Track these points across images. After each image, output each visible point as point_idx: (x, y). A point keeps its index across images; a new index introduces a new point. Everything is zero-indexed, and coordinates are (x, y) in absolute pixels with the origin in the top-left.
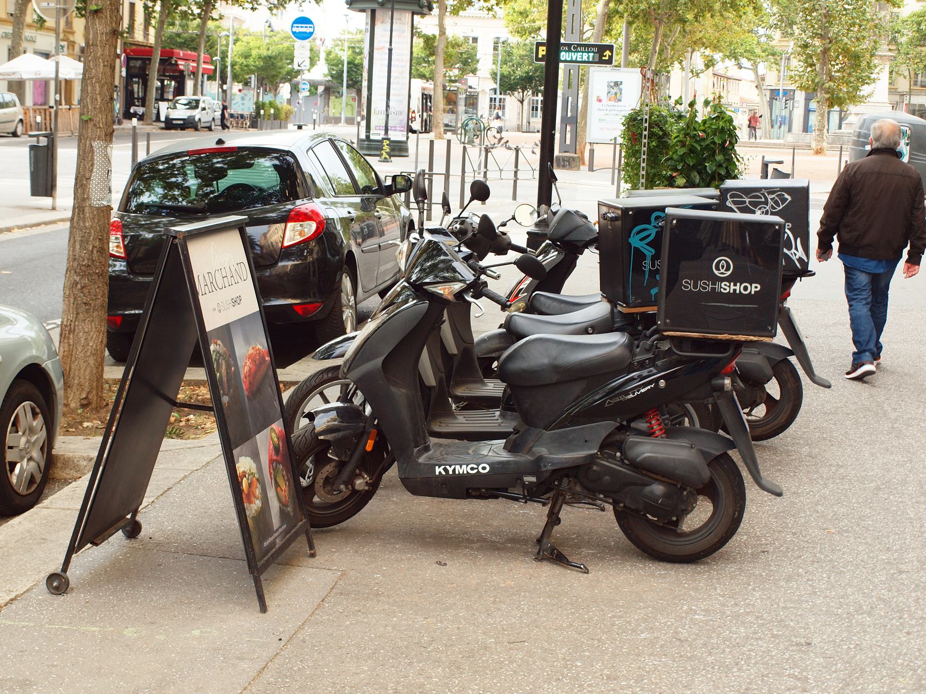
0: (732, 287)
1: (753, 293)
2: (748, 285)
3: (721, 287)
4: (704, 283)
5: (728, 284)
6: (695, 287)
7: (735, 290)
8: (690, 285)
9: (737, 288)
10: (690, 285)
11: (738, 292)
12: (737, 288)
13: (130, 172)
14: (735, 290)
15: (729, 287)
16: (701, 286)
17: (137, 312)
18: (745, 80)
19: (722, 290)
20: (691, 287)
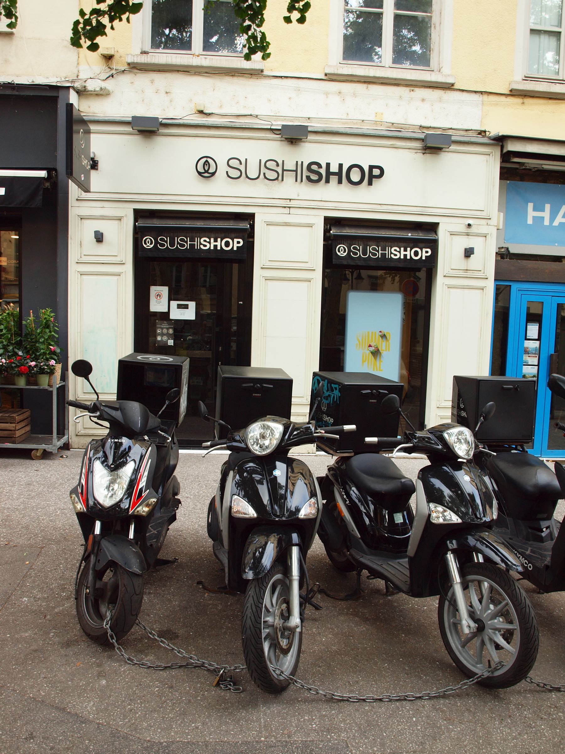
0: (403, 253)
1: (235, 249)
2: (230, 241)
3: (391, 253)
4: (373, 249)
5: (208, 240)
6: (172, 244)
7: (216, 246)
8: (359, 251)
9: (408, 253)
10: (359, 251)
11: (219, 248)
12: (408, 253)
13: (258, 68)
14: (216, 246)
15: (400, 252)
16: (370, 252)
17: (256, 395)
18: (80, 4)
19: (392, 256)
20: (360, 253)
